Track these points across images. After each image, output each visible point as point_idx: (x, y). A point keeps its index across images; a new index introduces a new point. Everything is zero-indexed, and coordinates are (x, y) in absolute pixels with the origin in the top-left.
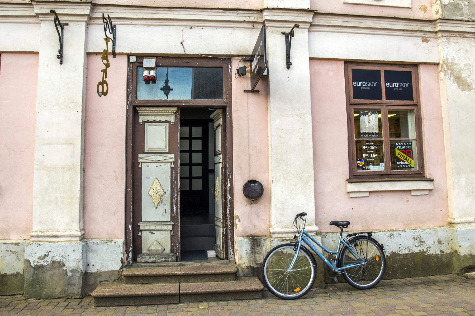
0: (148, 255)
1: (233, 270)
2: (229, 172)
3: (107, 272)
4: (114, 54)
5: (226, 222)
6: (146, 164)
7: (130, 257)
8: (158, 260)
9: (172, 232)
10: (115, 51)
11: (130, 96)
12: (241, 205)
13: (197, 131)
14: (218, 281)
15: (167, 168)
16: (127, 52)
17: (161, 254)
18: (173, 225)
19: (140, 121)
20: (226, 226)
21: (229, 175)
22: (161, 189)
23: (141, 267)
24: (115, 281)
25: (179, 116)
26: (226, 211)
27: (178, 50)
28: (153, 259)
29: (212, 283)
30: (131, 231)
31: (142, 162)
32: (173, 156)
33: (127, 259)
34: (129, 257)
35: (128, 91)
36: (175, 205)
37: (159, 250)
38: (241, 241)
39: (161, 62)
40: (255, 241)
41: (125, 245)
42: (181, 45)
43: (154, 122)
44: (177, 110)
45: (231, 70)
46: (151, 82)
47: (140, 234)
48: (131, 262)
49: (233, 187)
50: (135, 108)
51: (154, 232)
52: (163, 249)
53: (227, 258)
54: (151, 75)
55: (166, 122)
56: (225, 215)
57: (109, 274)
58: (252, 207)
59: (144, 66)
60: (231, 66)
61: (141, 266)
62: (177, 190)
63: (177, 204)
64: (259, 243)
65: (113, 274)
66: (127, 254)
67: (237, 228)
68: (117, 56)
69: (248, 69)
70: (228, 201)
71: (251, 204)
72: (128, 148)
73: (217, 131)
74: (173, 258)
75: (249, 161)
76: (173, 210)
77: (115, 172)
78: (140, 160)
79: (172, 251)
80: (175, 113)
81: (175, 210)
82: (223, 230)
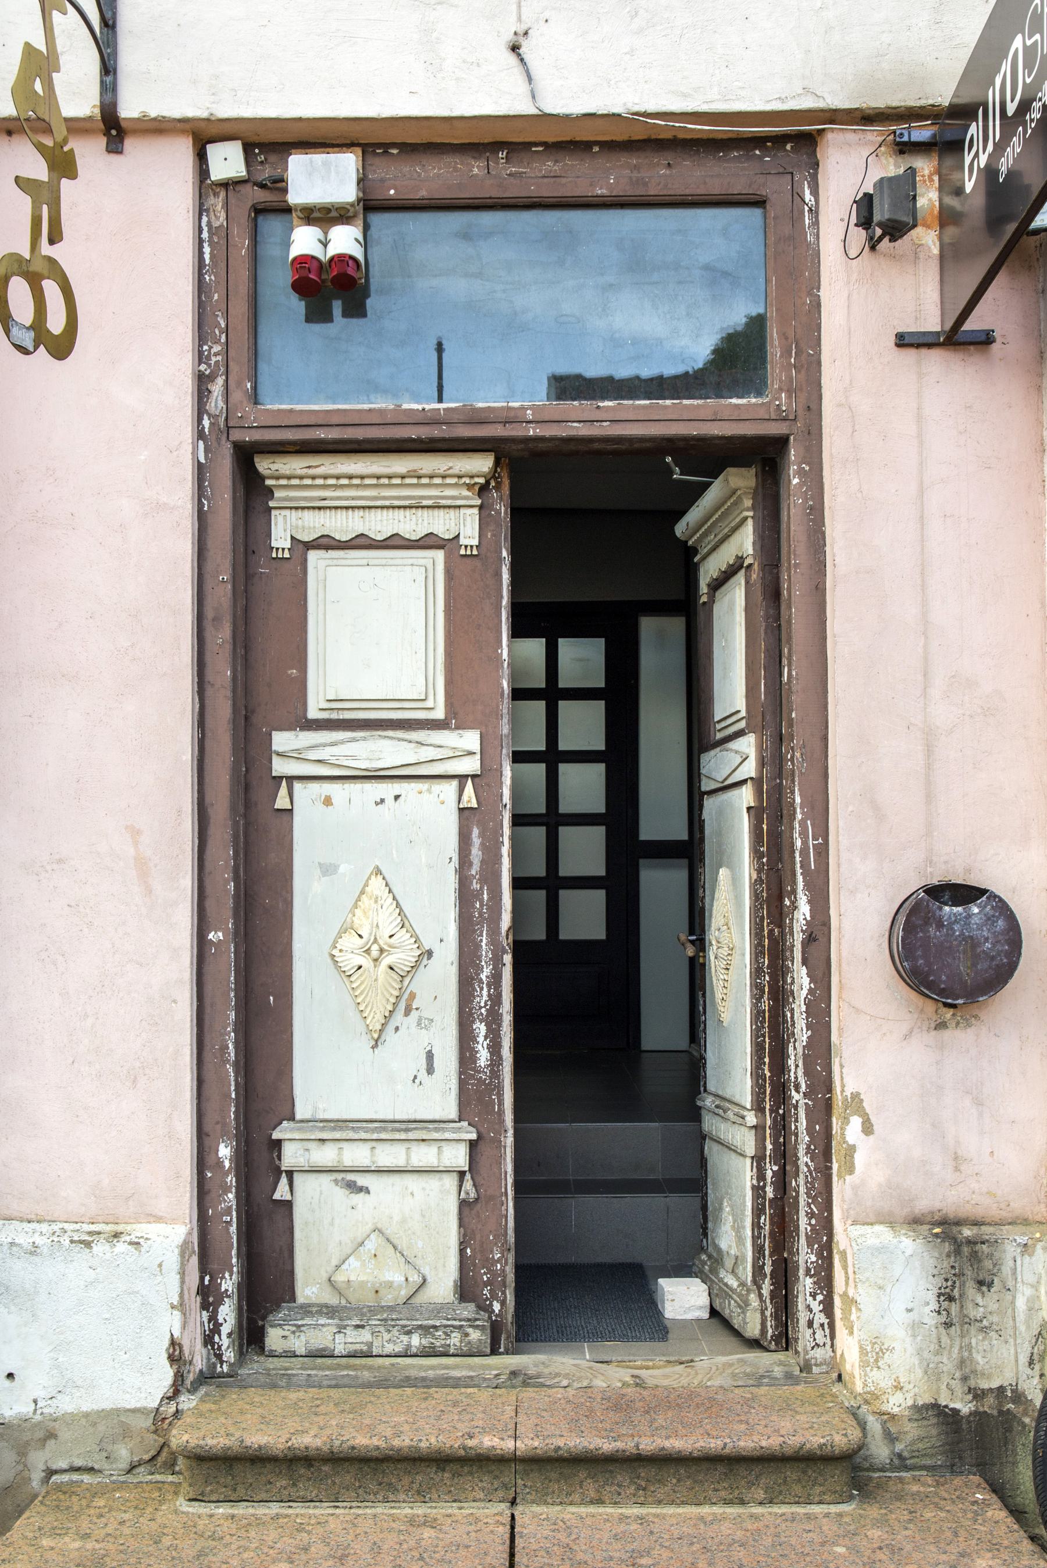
0: (330, 1311)
1: (840, 1437)
2: (804, 834)
3: (87, 1415)
4: (113, 129)
5: (782, 1126)
6: (314, 787)
7: (225, 1329)
8: (389, 1342)
9: (468, 1184)
10: (114, 105)
11: (217, 388)
12: (877, 1042)
13: (582, 659)
14: (742, 1502)
15: (436, 811)
16: (191, 113)
17: (404, 1311)
18: (473, 1145)
19: (280, 539)
20: (784, 1155)
21: (805, 852)
22: (403, 936)
23: (289, 1386)
24: (132, 1469)
25: (502, 509)
26: (779, 1065)
27: (489, 93)
28: (356, 1339)
29: (706, 1510)
30: (231, 1179)
31: (291, 779)
32: (471, 740)
33: (208, 1340)
34: (216, 1329)
35: (201, 357)
36: (481, 1029)
37: (390, 1285)
38: (881, 1250)
39: (401, 178)
40: (965, 1252)
41: (195, 1260)
42: (512, 59)
43: (362, 543)
44: (494, 475)
45: (815, 212)
46: (337, 307)
47: (282, 1192)
48: (229, 1355)
49: (826, 924)
50: (245, 457)
51: (361, 1180)
52: (415, 1278)
53: (785, 1340)
54: (333, 250)
55: (428, 542)
56: (774, 1088)
57: (101, 1428)
58: (941, 1047)
59: (294, 198)
60: (815, 192)
61: (290, 1382)
62: (494, 941)
63: (493, 1019)
64: (988, 1264)
65: (126, 1433)
66: (205, 1306)
67: (851, 1170)
68: (129, 143)
69: (928, 198)
70: (799, 1007)
71: (941, 1026)
72: (209, 692)
73: (719, 609)
74: (475, 1335)
75: (929, 767)
76: (474, 1053)
77: (135, 833)
78: (280, 767)
79: (465, 1290)
80: (483, 490)
81: (483, 1056)
82: (761, 1176)
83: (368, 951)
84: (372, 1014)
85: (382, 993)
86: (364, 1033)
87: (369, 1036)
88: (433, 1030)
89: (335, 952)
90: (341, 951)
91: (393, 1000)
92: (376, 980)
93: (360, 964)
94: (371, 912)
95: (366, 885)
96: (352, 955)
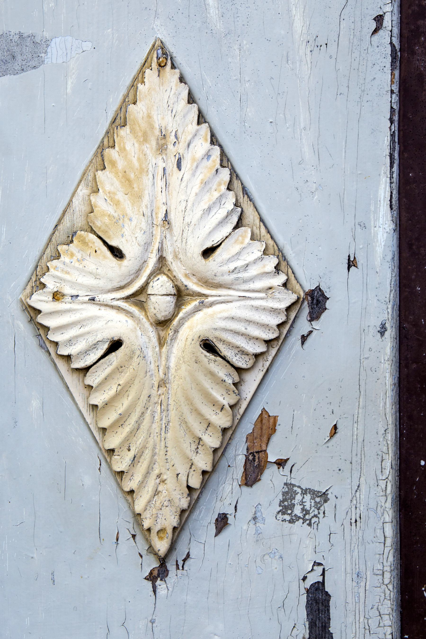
22: (243, 254)
83: (139, 298)
84: (152, 483)
85: (183, 422)
86: (125, 536)
87: (142, 547)
88: (326, 523)
89: (41, 300)
90: (57, 296)
91: (213, 441)
92: (163, 383)
93: (114, 333)
94: (147, 181)
95: (131, 97)
96: (92, 310)
